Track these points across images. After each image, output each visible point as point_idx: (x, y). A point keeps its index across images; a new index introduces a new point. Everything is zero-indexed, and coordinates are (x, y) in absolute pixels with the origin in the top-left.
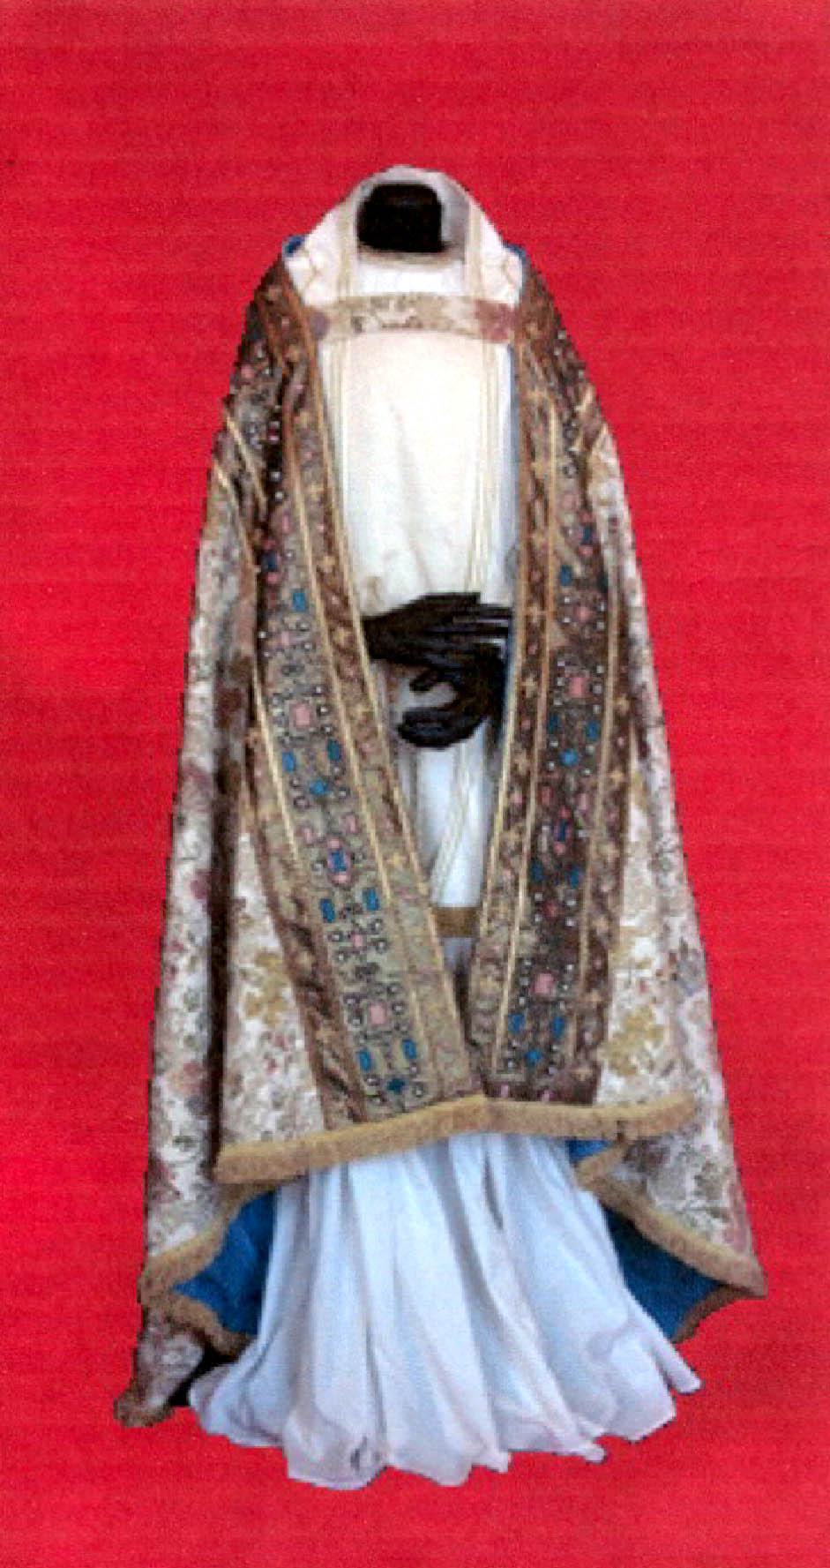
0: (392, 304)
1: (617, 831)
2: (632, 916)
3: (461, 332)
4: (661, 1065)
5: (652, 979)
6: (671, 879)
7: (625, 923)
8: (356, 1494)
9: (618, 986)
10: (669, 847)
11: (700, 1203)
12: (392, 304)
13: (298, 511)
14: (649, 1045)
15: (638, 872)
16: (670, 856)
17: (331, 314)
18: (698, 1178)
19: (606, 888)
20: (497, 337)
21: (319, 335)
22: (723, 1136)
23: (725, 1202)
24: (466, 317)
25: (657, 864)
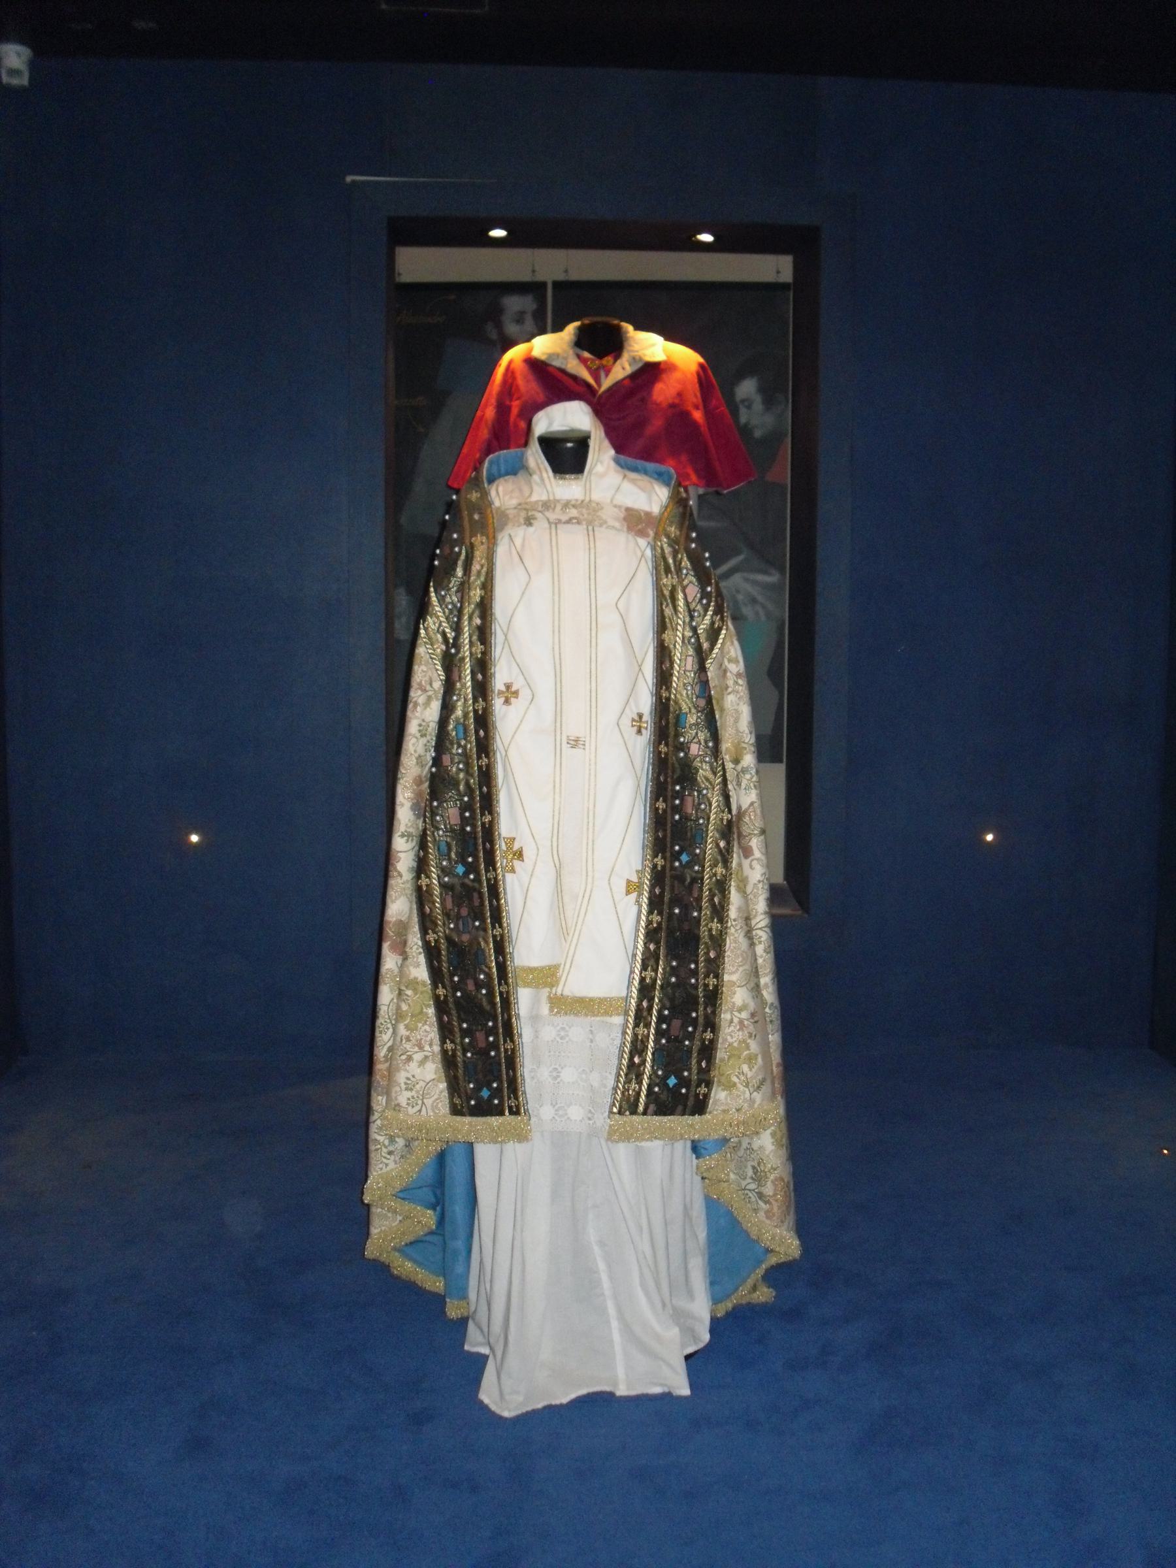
0: (559, 507)
1: (720, 912)
2: (731, 974)
3: (613, 527)
4: (755, 1082)
5: (747, 1020)
6: (760, 949)
7: (726, 978)
8: (506, 1419)
9: (724, 1024)
10: (759, 926)
11: (753, 1186)
12: (559, 507)
13: (484, 464)
14: (745, 1068)
15: (735, 941)
16: (760, 933)
17: (511, 513)
18: (754, 1168)
19: (712, 955)
20: (642, 533)
21: (503, 526)
22: (778, 1144)
23: (769, 1190)
24: (617, 519)
25: (749, 934)
